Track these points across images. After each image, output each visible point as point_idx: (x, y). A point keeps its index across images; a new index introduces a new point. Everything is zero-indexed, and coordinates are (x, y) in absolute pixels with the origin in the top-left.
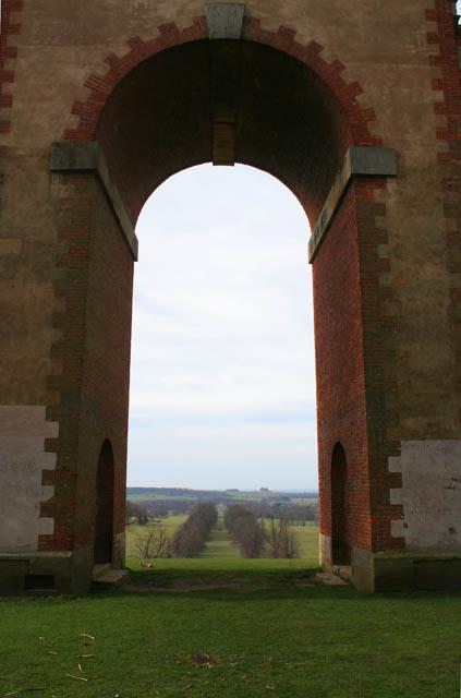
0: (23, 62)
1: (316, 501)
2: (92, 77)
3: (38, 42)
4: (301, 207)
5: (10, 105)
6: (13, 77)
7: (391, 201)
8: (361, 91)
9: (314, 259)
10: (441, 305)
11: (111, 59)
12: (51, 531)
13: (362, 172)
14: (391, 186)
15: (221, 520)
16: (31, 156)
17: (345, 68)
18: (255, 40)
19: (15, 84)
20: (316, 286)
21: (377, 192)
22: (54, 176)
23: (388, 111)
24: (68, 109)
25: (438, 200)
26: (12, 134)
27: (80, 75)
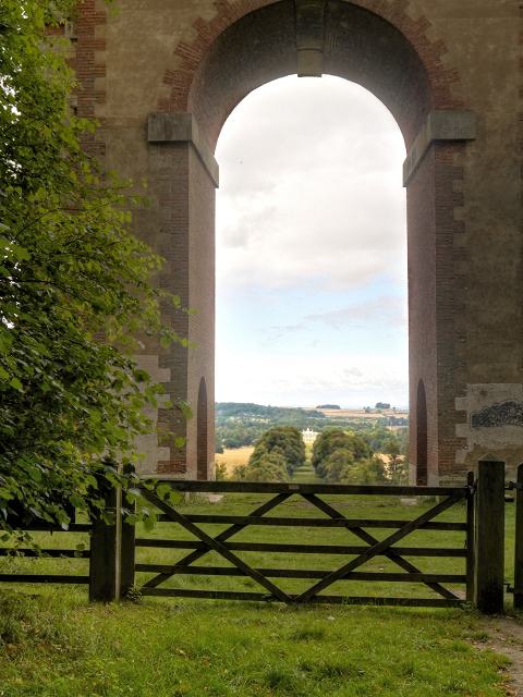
0: (113, 29)
1: (406, 417)
2: (181, 44)
3: (126, 6)
4: (391, 115)
5: (104, 75)
6: (105, 44)
7: (469, 164)
8: (446, 51)
9: (406, 185)
10: (511, 263)
11: (199, 24)
12: (167, 458)
13: (443, 137)
14: (470, 150)
15: (309, 455)
16: (128, 127)
17: (430, 24)
18: (39, 584)
19: (107, 52)
20: (408, 233)
21: (456, 156)
22: (151, 147)
23: (472, 71)
24: (160, 79)
25: (516, 162)
26: (109, 104)
27: (169, 42)
